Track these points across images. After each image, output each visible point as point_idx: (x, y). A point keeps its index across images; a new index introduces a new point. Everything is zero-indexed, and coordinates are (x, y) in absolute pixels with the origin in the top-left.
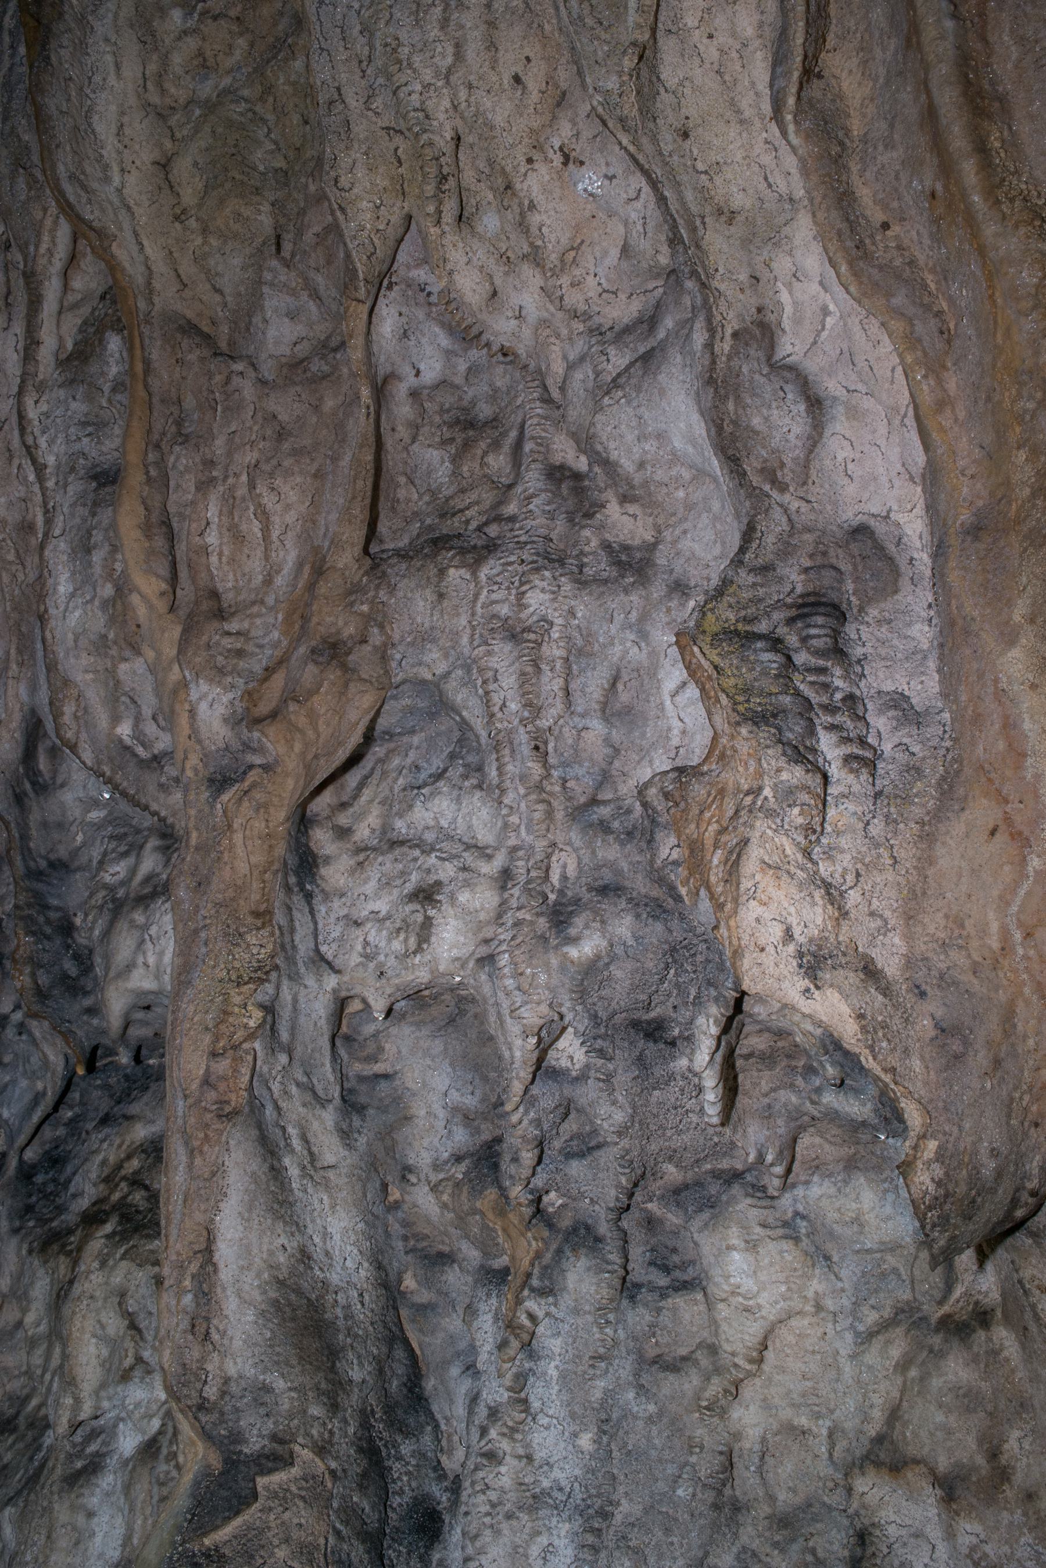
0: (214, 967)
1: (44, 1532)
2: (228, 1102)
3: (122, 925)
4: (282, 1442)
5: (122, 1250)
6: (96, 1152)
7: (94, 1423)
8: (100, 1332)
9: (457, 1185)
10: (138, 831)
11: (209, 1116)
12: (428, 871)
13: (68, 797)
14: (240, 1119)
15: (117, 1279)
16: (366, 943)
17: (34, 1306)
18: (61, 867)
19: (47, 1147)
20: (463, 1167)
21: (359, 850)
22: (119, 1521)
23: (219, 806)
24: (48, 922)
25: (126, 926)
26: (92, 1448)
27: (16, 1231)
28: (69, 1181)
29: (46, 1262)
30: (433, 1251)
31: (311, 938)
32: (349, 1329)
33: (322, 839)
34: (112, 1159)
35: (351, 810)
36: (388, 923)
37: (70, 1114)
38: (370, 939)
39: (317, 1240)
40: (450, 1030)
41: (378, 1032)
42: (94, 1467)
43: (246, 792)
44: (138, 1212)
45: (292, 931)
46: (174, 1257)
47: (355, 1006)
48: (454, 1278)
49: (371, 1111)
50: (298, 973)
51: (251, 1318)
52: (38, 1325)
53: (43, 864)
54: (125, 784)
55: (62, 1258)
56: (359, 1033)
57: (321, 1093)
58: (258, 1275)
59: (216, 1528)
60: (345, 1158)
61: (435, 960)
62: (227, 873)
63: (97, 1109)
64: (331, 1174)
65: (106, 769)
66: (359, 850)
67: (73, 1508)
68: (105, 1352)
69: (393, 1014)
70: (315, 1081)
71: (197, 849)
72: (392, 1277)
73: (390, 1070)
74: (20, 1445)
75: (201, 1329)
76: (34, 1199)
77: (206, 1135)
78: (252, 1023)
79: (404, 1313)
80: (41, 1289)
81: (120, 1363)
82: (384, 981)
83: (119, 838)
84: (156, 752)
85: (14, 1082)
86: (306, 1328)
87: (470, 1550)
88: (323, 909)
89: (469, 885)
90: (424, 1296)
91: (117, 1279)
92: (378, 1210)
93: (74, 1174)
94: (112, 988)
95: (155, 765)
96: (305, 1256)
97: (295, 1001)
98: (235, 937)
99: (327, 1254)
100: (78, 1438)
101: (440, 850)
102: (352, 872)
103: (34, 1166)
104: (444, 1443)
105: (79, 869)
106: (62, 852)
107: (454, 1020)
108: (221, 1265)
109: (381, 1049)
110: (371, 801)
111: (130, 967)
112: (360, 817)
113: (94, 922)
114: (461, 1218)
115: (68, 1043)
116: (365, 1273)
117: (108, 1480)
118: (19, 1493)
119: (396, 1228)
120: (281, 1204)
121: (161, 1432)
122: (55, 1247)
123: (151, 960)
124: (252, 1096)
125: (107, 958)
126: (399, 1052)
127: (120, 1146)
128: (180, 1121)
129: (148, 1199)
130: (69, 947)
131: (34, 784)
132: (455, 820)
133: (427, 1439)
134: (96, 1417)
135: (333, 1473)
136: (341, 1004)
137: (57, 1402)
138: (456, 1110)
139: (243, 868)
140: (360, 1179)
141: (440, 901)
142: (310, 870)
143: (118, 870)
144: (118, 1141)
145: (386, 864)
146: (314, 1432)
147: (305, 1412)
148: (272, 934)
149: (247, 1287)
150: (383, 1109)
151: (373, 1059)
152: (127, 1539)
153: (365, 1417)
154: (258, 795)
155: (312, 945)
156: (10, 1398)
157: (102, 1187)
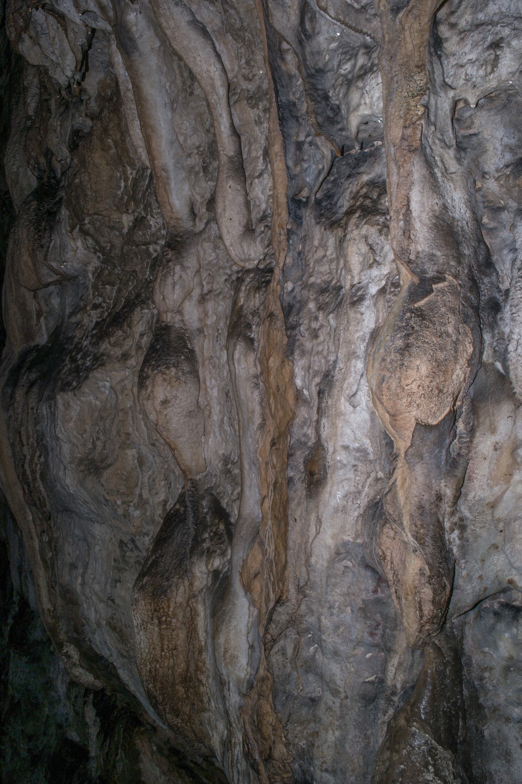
0: (401, 92)
1: (346, 320)
2: (412, 146)
3: (353, 89)
4: (441, 273)
5: (364, 221)
6: (347, 188)
7: (359, 285)
8: (358, 252)
9: (508, 176)
10: (354, 49)
11: (405, 152)
12: (497, 34)
13: (321, 39)
14: (418, 152)
15: (364, 232)
16: (466, 74)
17: (330, 248)
18: (321, 71)
19: (325, 192)
20: (510, 169)
21: (461, 33)
22: (373, 315)
23: (397, 20)
24: (319, 96)
25: (355, 89)
26: (359, 293)
27: (318, 223)
28: (336, 203)
29: (332, 232)
30: (495, 207)
31: (441, 75)
32: (463, 235)
33: (444, 31)
34: (354, 190)
35: (457, 14)
36: (477, 63)
37: (332, 178)
38: (469, 72)
39: (449, 201)
40: (504, 110)
41: (472, 115)
42: (362, 299)
43: (409, 11)
44: (368, 208)
45: (433, 73)
46: (395, 208)
47: (461, 105)
48: (505, 216)
49: (469, 150)
50: (437, 91)
51: (426, 230)
52: (332, 255)
53: (313, 71)
54: (350, 22)
55: (339, 229)
56: (463, 117)
57: (448, 143)
58: (428, 214)
59: (419, 301)
60: (459, 169)
61: (500, 75)
62: (403, 51)
63: (344, 174)
64: (454, 176)
65: (341, 17)
66: (461, 33)
67: (355, 312)
68: (361, 259)
69: (479, 106)
70: (445, 138)
71: (389, 42)
72: (479, 217)
73: (476, 132)
74: (332, 296)
75: (407, 235)
76: (323, 211)
77: (405, 160)
78: (420, 113)
79: (483, 232)
80: (331, 242)
81: (368, 262)
82: (476, 89)
83: (345, 53)
84: (363, 4)
85: (310, 167)
86: (447, 233)
87: (514, 310)
88: (446, 62)
89: (517, 36)
90: (492, 225)
91: (364, 232)
92: (473, 191)
93: (338, 200)
94: (352, 115)
95: (363, 10)
96: (445, 207)
97: (436, 103)
98: (409, 78)
99: (453, 207)
100: (353, 290)
101: (502, 23)
102: (458, 43)
103: (320, 200)
104: (500, 280)
105: (329, 71)
106: (321, 65)
107: (506, 106)
108: (413, 211)
109: (473, 123)
110: (466, 8)
111: (358, 106)
112: (461, 16)
113: (339, 92)
114: (509, 190)
115: (332, 145)
116: (468, 215)
117: (367, 303)
118: (334, 310)
119: (479, 198)
120: (435, 187)
121: (386, 285)
122: (336, 225)
123: (368, 101)
124: (422, 144)
125: (348, 104)
126: (481, 123)
127: (357, 185)
128: (393, 156)
129: (372, 202)
130: (328, 105)
131: (305, 35)
132: (509, 7)
133: (494, 278)
134: (360, 283)
135: (460, 285)
136: (455, 103)
137: (345, 278)
138: (506, 146)
139: (410, 47)
140: (465, 178)
141: (503, 47)
142: (439, 45)
143: (348, 66)
144: (356, 183)
145: (476, 36)
146: (453, 270)
147: (449, 263)
148: (426, 74)
149: (424, 219)
150: (474, 149)
151: (469, 127)
152: (377, 321)
153: (470, 268)
154: (415, 12)
155: (442, 79)
156: (324, 282)
157: (351, 201)
